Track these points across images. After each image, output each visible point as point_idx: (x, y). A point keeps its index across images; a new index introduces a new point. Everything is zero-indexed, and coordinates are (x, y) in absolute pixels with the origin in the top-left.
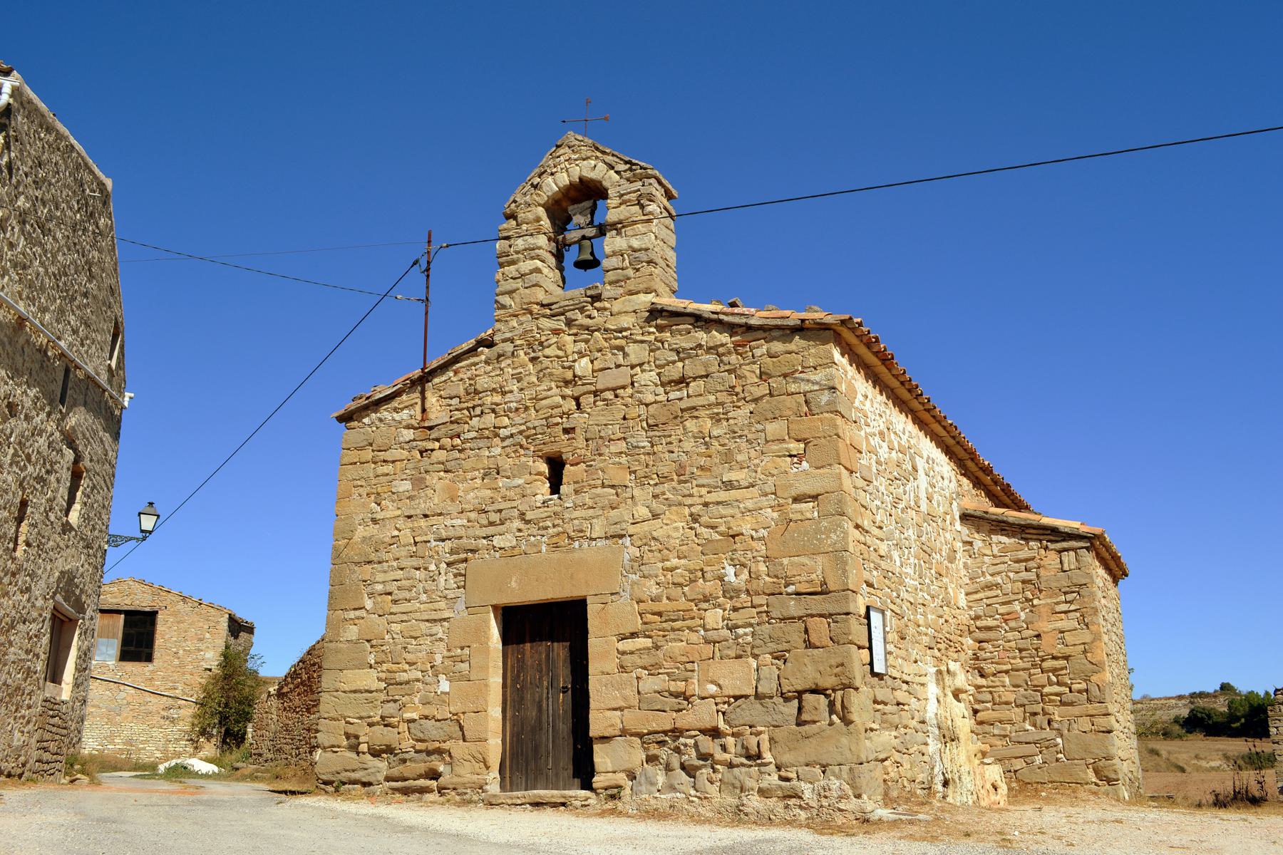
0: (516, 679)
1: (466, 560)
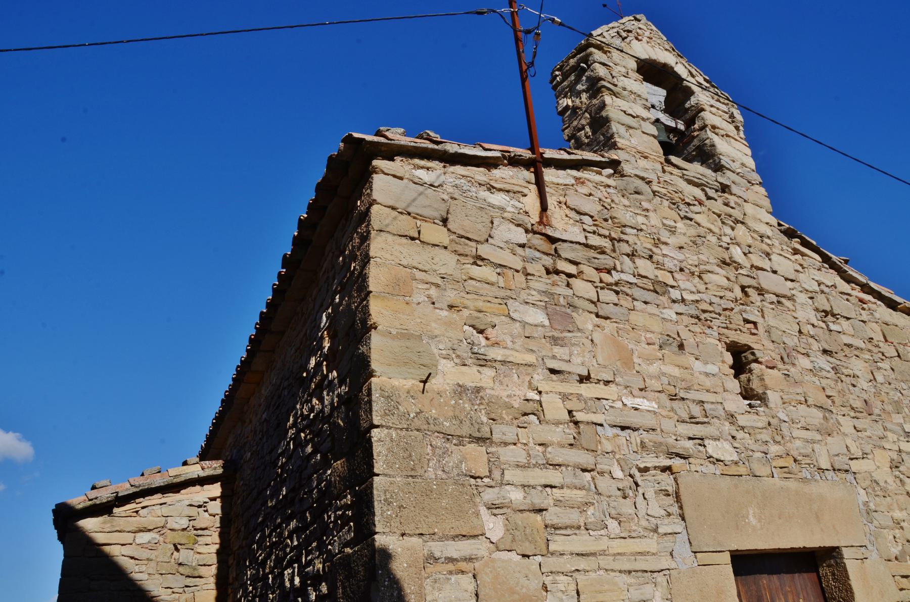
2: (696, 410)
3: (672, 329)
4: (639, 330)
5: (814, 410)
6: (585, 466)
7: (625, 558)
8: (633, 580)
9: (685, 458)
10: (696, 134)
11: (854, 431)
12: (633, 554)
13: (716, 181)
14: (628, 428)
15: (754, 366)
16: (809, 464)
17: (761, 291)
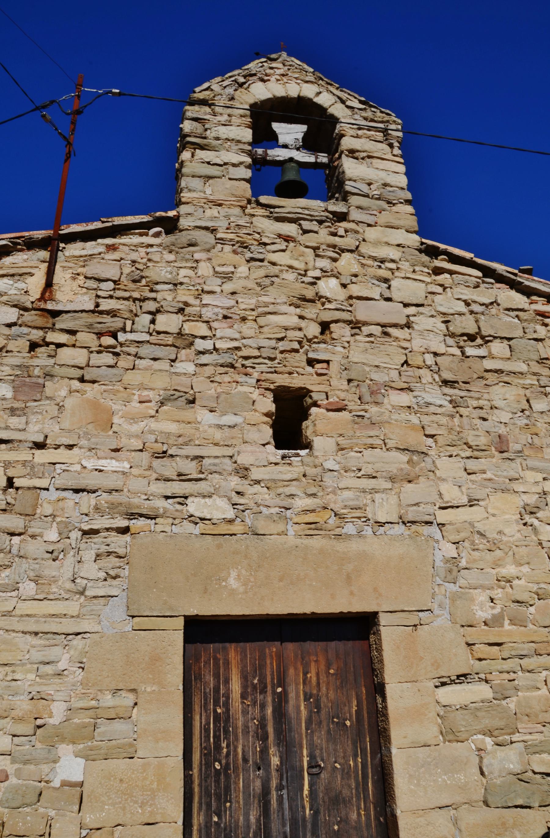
0: (211, 754)
1: (125, 531)
2: (191, 468)
3: (183, 383)
4: (133, 389)
5: (394, 454)
6: (12, 530)
7: (33, 620)
8: (42, 642)
9: (152, 519)
10: (336, 163)
11: (465, 474)
12: (45, 616)
13: (326, 210)
14: (83, 490)
15: (314, 410)
16: (359, 518)
17: (356, 325)
